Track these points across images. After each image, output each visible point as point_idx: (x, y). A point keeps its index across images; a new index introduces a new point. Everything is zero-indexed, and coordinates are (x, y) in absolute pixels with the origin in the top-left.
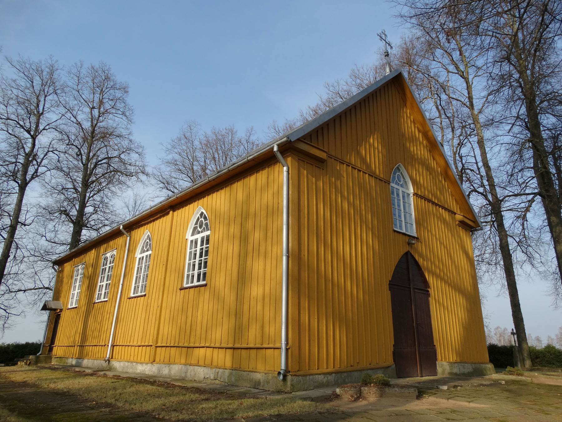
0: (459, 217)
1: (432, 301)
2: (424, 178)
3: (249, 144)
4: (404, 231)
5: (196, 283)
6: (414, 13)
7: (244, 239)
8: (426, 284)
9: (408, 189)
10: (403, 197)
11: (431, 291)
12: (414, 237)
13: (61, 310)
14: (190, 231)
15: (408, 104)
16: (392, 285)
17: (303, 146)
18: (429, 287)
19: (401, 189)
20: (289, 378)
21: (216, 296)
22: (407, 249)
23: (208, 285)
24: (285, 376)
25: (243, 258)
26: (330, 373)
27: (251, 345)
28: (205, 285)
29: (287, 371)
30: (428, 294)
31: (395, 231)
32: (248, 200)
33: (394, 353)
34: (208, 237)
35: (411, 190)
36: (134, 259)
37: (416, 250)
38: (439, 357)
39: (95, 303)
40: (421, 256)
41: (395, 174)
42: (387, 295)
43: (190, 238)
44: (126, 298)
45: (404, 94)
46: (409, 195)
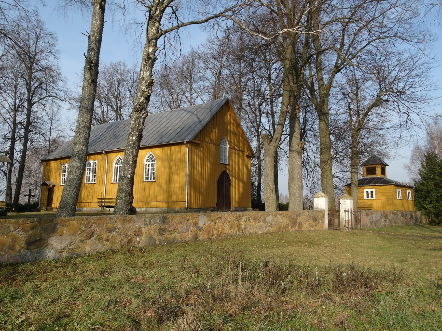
0: (246, 153)
1: (231, 187)
2: (233, 139)
3: (135, 73)
4: (224, 163)
5: (150, 180)
6: (238, 65)
7: (170, 168)
8: (230, 181)
9: (227, 146)
10: (225, 149)
11: (232, 183)
12: (227, 165)
13: (54, 186)
14: (145, 160)
15: (230, 110)
16: (218, 182)
17: (194, 141)
18: (231, 182)
19: (224, 147)
20: (188, 209)
21: (160, 186)
22: (224, 169)
23: (156, 181)
24: (187, 209)
25: (170, 174)
26: (198, 208)
27: (172, 201)
28: (155, 182)
29: (187, 207)
30: (230, 184)
31: (221, 163)
32: (171, 155)
33: (217, 204)
34: (154, 164)
35: (228, 146)
36: (112, 167)
37: (228, 169)
38: (232, 205)
39: (85, 184)
40: (229, 171)
41: (223, 140)
42: (216, 186)
43: (146, 163)
44: (109, 183)
45: (229, 106)
46: (227, 148)
